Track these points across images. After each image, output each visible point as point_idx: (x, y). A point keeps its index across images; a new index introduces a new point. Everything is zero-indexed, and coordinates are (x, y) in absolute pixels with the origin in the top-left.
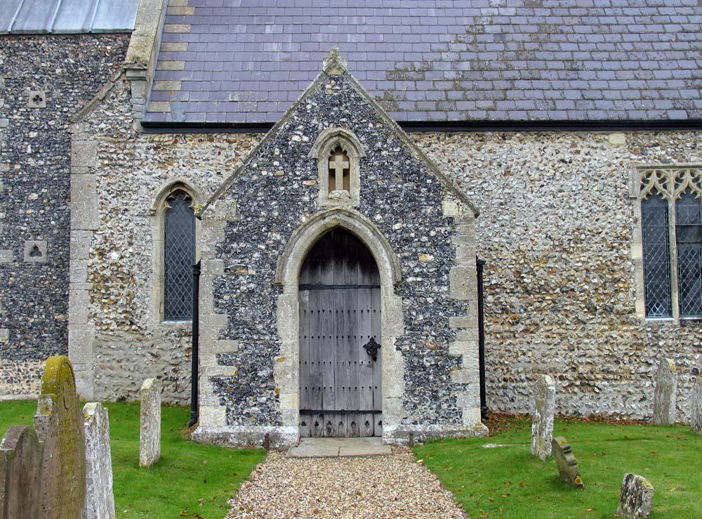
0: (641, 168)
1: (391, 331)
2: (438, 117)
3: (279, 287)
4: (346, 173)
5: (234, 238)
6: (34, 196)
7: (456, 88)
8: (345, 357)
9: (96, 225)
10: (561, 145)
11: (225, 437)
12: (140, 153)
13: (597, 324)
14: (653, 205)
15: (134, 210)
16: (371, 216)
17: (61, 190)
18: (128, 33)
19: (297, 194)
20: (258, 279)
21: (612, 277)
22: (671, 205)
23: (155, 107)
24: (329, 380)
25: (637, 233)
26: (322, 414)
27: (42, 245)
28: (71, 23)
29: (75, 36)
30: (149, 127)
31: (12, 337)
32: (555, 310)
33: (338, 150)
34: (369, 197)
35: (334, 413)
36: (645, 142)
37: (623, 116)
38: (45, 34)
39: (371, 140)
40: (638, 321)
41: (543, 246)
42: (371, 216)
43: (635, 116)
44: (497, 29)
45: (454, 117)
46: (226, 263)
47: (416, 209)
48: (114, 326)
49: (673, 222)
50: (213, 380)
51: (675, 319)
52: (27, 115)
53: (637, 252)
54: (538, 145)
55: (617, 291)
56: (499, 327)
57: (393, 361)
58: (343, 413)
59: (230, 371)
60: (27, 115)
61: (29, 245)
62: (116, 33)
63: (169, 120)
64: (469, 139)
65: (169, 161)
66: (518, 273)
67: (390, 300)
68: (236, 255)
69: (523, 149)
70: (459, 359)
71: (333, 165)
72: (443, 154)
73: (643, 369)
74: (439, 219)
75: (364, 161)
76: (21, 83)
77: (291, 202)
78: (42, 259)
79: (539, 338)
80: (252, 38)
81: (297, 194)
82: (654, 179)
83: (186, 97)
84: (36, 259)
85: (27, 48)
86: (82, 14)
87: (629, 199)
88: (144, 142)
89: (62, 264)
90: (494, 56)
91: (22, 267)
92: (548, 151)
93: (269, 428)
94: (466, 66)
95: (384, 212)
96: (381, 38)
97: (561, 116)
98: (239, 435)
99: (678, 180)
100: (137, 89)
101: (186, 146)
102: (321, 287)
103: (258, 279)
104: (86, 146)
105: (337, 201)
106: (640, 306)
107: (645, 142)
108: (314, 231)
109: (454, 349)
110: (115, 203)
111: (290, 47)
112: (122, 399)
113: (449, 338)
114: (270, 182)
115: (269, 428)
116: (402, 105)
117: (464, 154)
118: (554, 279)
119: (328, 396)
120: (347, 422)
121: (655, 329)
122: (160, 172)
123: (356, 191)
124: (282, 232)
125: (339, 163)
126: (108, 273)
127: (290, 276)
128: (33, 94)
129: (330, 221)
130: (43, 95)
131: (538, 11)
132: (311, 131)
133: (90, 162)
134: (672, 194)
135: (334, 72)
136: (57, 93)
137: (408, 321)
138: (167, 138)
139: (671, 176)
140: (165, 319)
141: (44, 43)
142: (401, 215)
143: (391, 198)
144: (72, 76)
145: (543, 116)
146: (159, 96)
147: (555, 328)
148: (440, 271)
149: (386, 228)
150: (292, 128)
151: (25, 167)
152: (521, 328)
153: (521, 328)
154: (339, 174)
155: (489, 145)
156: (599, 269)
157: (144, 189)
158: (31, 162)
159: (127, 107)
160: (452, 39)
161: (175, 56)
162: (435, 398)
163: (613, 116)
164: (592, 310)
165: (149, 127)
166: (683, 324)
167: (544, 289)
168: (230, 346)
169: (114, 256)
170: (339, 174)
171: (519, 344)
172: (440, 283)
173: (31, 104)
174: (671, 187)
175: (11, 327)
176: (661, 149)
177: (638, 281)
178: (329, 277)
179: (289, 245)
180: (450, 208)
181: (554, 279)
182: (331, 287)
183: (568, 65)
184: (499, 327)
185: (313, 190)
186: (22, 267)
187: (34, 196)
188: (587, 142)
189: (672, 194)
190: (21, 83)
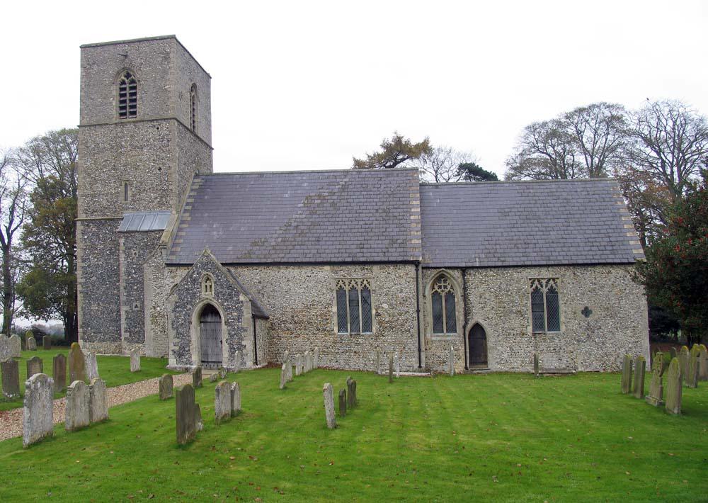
0: (335, 279)
1: (224, 336)
2: (264, 261)
3: (190, 323)
4: (211, 286)
5: (177, 307)
6: (135, 288)
7: (274, 249)
8: (214, 345)
9: (152, 298)
10: (306, 271)
11: (176, 368)
12: (166, 274)
13: (320, 335)
14: (341, 293)
16: (218, 300)
17: (142, 290)
18: (163, 230)
19: (196, 293)
20: (185, 320)
21: (327, 319)
22: (347, 293)
23: (171, 257)
24: (210, 352)
25: (335, 302)
26: (208, 362)
28: (145, 228)
29: (147, 232)
30: (168, 265)
31: (130, 335)
32: (305, 330)
33: (208, 279)
34: (217, 294)
35: (212, 362)
36: (337, 269)
37: (329, 260)
38: (137, 231)
39: (217, 276)
40: (335, 334)
41: (301, 306)
42: (218, 300)
43: (333, 260)
44: (296, 224)
45: (269, 261)
46: (175, 315)
47: (231, 298)
48: (159, 333)
49: (348, 299)
50: (173, 351)
51: (348, 333)
53: (335, 309)
54: (299, 270)
55: (328, 323)
56: (286, 335)
57: (226, 346)
58: (214, 362)
59: (177, 348)
61: (134, 304)
62: (159, 231)
63: (174, 262)
64: (275, 268)
65: (175, 276)
66: (292, 316)
67: (224, 327)
68: (178, 312)
69: (294, 272)
70: (245, 346)
71: (207, 284)
73: (336, 351)
74: (238, 301)
75: (215, 283)
77: (194, 295)
78: (138, 309)
79: (300, 339)
80: (208, 229)
81: (196, 293)
83: (181, 254)
84: (136, 309)
85: (131, 236)
89: (143, 311)
90: (291, 235)
91: (133, 312)
92: (303, 272)
93: (188, 366)
94: (280, 240)
95: (221, 299)
96: (253, 229)
97: (307, 260)
98: (180, 368)
99: (362, 283)
100: (164, 251)
102: (207, 322)
103: (185, 320)
104: (149, 272)
105: (207, 295)
106: (336, 329)
107: (337, 269)
108: (201, 305)
109: (244, 343)
110: (158, 291)
111: (221, 233)
112: (162, 357)
113: (242, 340)
114: (188, 289)
115: (188, 366)
116: (253, 256)
117: (273, 273)
118: (305, 319)
119: (210, 357)
120: (216, 365)
121: (341, 337)
122: (172, 280)
124: (191, 305)
125: (208, 284)
126: (156, 314)
127: (194, 318)
128: (134, 252)
129: (205, 302)
130: (137, 252)
131: (314, 216)
132: (199, 273)
133: (150, 277)
134: (347, 288)
135: (206, 254)
136: (141, 252)
137: (229, 334)
138: (174, 269)
140: (434, 332)
141: (137, 234)
142: (227, 300)
143: (224, 295)
145: (299, 260)
146: (173, 253)
147: (306, 336)
148: (239, 318)
149: (222, 304)
150: (194, 272)
151: (132, 278)
152: (293, 336)
153: (293, 336)
154: (208, 287)
155: (282, 271)
156: (321, 315)
157: (167, 286)
158: (134, 275)
159: (162, 258)
160: (278, 228)
161: (181, 237)
163: (325, 260)
164: (319, 330)
165: (168, 265)
166: (351, 335)
167: (301, 322)
168: (177, 340)
169: (158, 309)
170: (208, 287)
171: (293, 341)
172: (239, 322)
173: (134, 256)
174: (347, 286)
175: (130, 332)
176: (343, 272)
177: (335, 320)
178: (209, 319)
179: (193, 310)
180: (242, 298)
181: (305, 319)
182: (210, 322)
183: (317, 239)
184: (286, 335)
185: (200, 292)
186: (133, 312)
187: (135, 288)
189: (347, 288)
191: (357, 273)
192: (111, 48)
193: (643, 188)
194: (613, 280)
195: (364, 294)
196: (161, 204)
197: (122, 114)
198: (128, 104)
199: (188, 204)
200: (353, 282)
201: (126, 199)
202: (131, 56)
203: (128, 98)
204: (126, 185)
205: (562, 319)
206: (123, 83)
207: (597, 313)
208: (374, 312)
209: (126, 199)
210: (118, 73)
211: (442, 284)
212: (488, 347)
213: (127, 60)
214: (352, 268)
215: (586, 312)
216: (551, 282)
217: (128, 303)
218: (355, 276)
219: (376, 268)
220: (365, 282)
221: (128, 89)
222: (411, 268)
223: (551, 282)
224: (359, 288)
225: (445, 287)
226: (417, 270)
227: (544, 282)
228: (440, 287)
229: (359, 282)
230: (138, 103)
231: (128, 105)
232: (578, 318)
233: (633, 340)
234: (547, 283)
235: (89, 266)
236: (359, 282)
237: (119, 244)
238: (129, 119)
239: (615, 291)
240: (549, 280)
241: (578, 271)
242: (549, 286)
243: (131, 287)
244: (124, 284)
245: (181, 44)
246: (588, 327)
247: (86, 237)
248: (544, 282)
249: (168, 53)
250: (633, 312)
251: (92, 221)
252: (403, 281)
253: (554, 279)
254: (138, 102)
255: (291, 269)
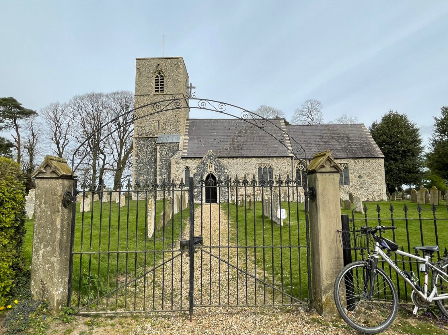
10: (246, 160)
14: (260, 169)
15: (180, 171)
19: (205, 169)
27: (166, 176)
28: (170, 141)
30: (183, 158)
34: (215, 169)
38: (166, 143)
39: (215, 161)
52: (163, 155)
60: (163, 155)
62: (177, 143)
72: (224, 161)
74: (225, 172)
76: (162, 150)
81: (205, 169)
82: (260, 165)
86: (171, 139)
87: (256, 168)
88: (182, 160)
101: (188, 161)
104: (173, 160)
108: (207, 174)
110: (178, 169)
114: (201, 168)
123: (213, 169)
125: (211, 165)
129: (209, 173)
134: (263, 167)
139: (263, 164)
144: (170, 149)
162: (224, 197)
165: (183, 158)
169: (177, 177)
176: (261, 160)
188: (250, 160)
189: (263, 167)
190: (162, 150)
191: (267, 161)
192: (151, 60)
193: (193, 129)
194: (371, 164)
195: (270, 170)
196: (176, 131)
197: (156, 91)
198: (160, 86)
199: (186, 132)
200: (265, 165)
201: (159, 129)
202: (161, 65)
203: (159, 84)
204: (159, 122)
205: (350, 180)
206: (157, 77)
207: (365, 178)
208: (274, 177)
209: (159, 129)
210: (155, 72)
211: (301, 166)
212: (75, 236)
213: (159, 67)
214: (265, 159)
215: (360, 177)
216: (346, 165)
217: (161, 175)
218: (266, 162)
219: (275, 159)
220: (270, 165)
221: (159, 80)
222: (289, 159)
223: (346, 165)
224: (268, 167)
225: (302, 167)
226: (292, 160)
227: (343, 165)
228: (299, 167)
229: (268, 164)
230: (165, 86)
231: (160, 86)
232: (357, 179)
233: (379, 188)
234: (344, 165)
235: (139, 159)
236: (268, 164)
237: (156, 149)
238: (160, 93)
239: (372, 168)
240: (345, 164)
241: (357, 160)
242: (345, 166)
243: (162, 168)
244: (159, 167)
245: (172, 58)
246: (361, 183)
247: (138, 145)
248: (343, 165)
249: (179, 65)
250: (379, 177)
251: (141, 138)
252: (286, 164)
253: (346, 164)
254: (165, 86)
255: (238, 159)
